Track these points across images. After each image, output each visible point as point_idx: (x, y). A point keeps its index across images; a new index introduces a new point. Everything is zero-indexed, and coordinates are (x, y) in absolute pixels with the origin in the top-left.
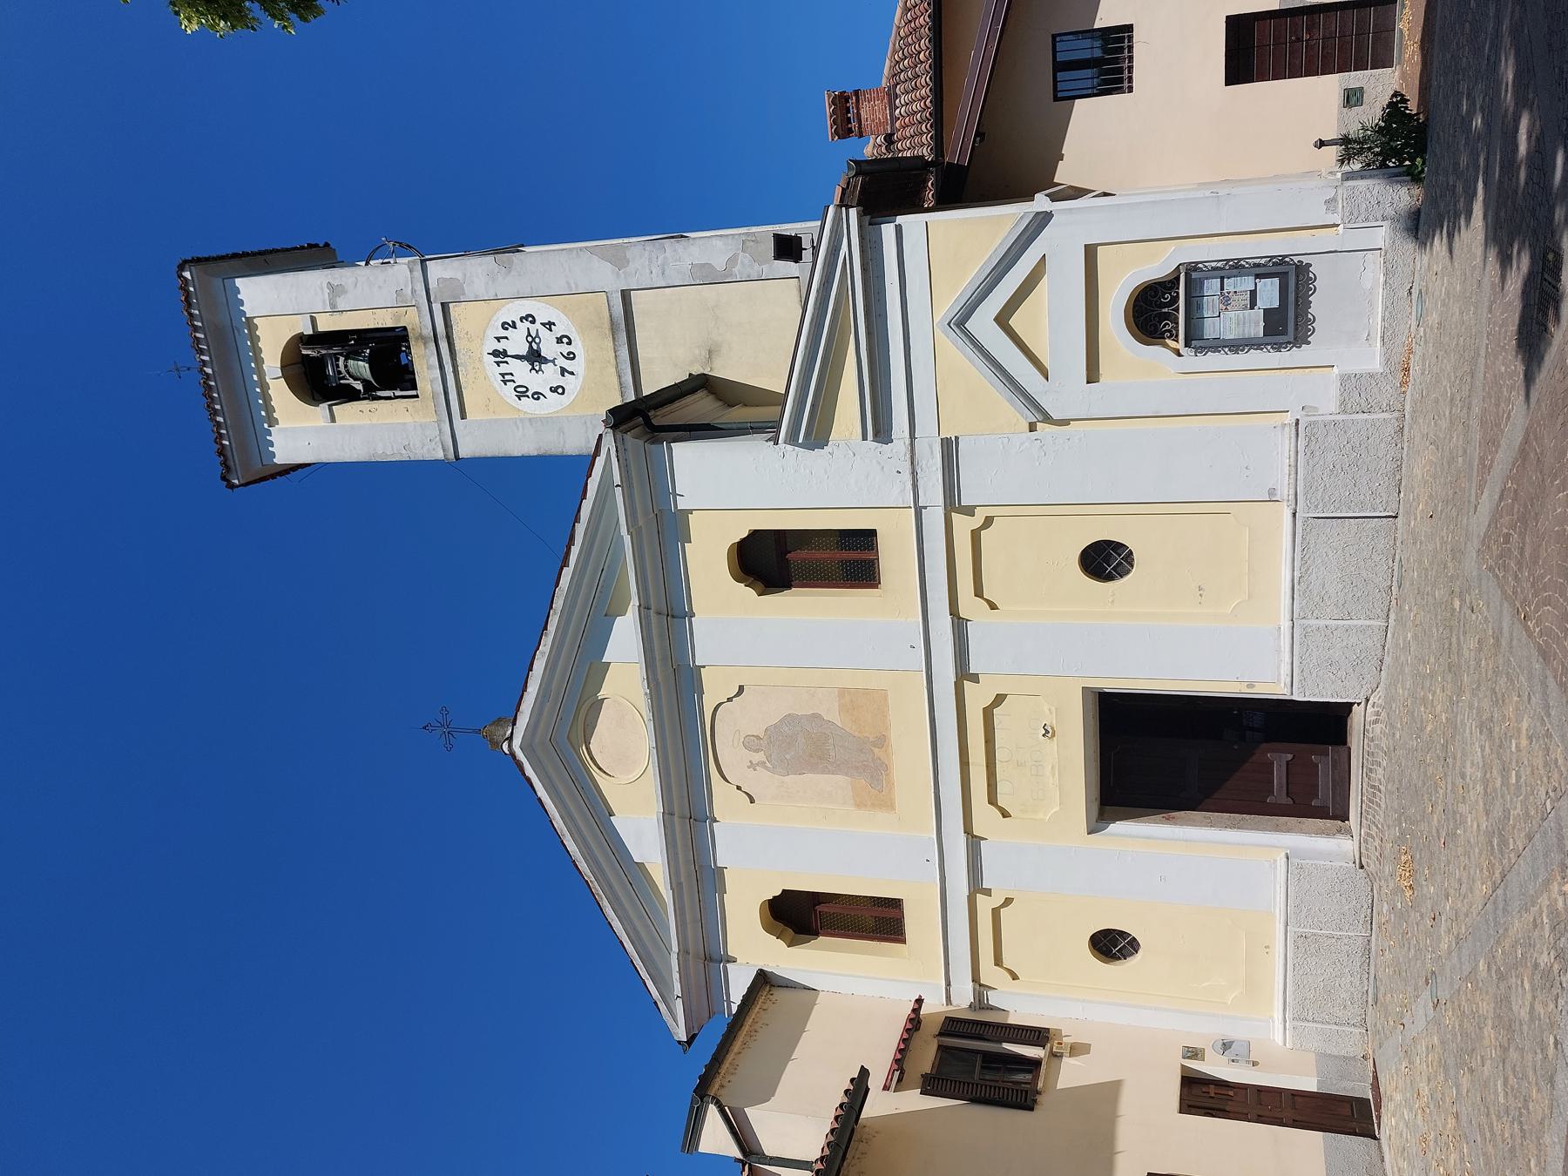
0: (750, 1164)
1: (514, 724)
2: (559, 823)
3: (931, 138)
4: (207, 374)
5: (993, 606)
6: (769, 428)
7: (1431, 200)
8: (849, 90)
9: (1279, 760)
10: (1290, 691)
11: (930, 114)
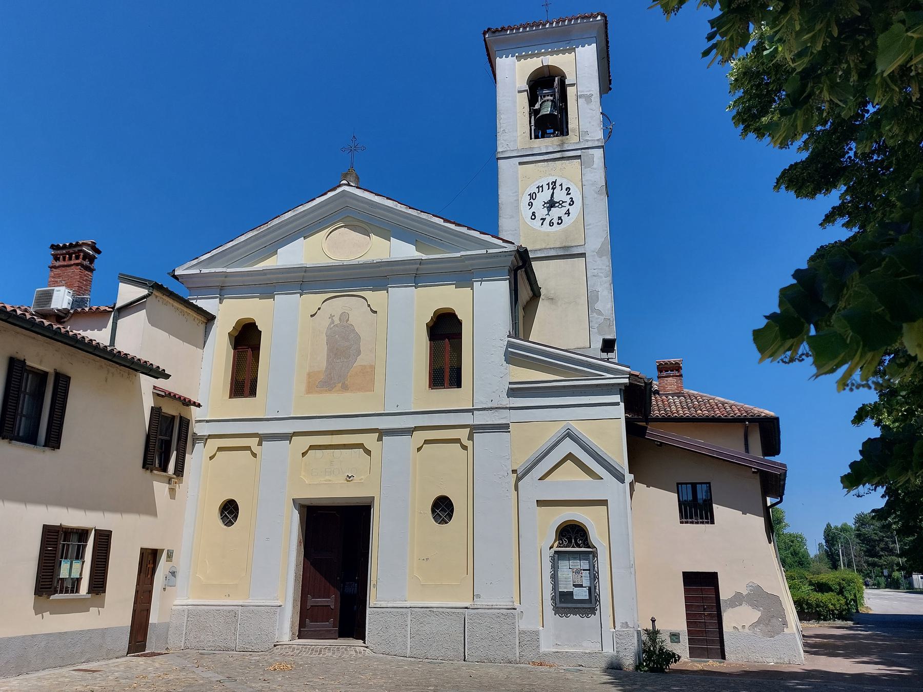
0: (112, 311)
1: (357, 188)
2: (301, 209)
3: (657, 416)
4: (546, 25)
5: (419, 449)
6: (515, 333)
7: (627, 675)
8: (682, 372)
9: (331, 601)
10: (372, 606)
11: (670, 416)
